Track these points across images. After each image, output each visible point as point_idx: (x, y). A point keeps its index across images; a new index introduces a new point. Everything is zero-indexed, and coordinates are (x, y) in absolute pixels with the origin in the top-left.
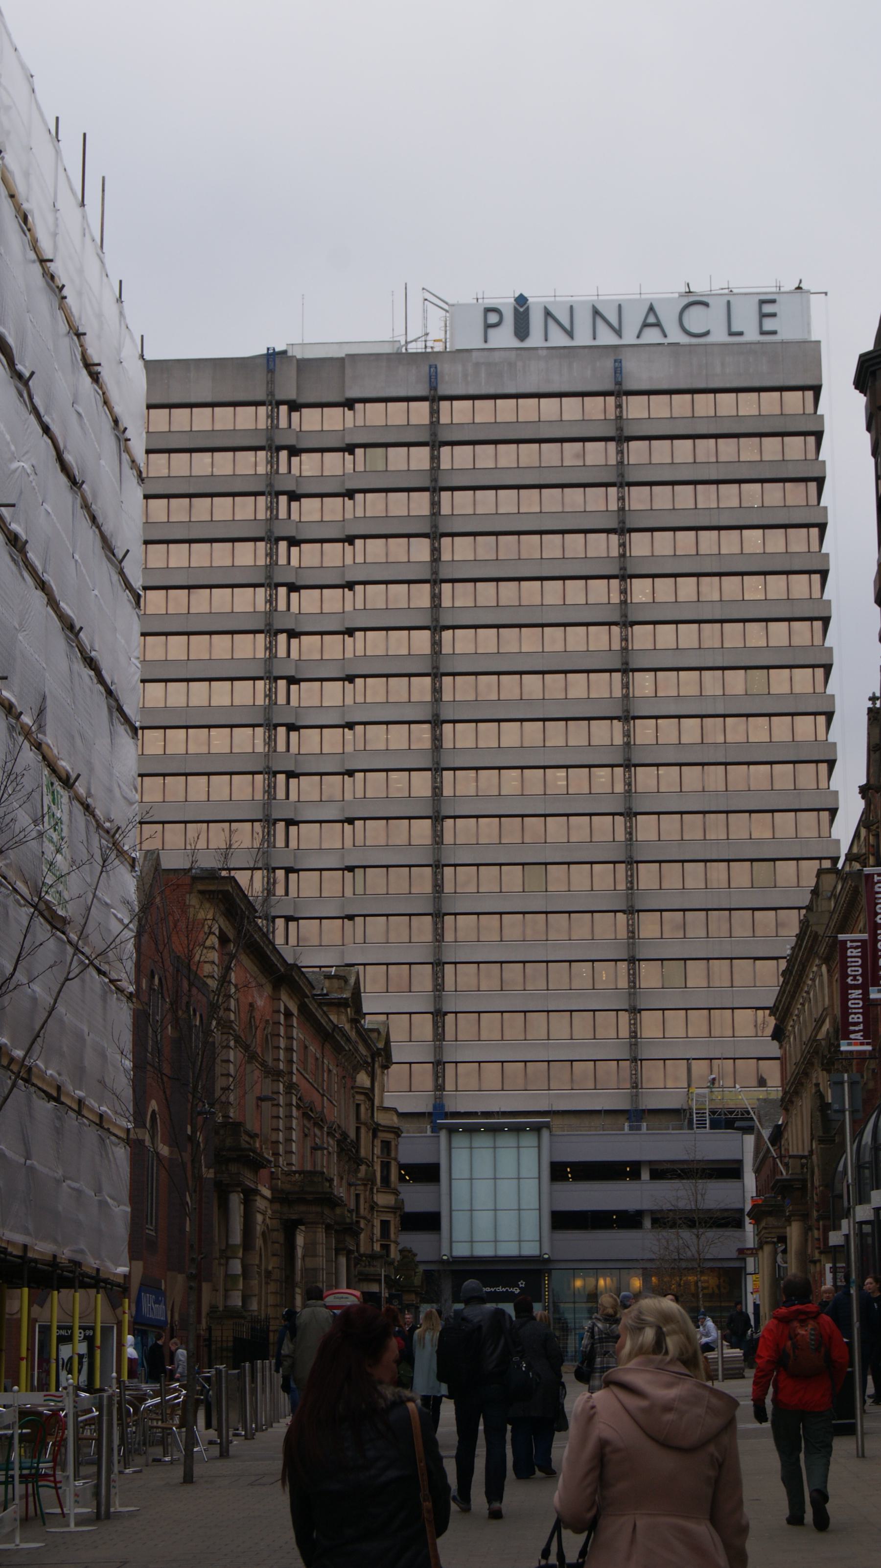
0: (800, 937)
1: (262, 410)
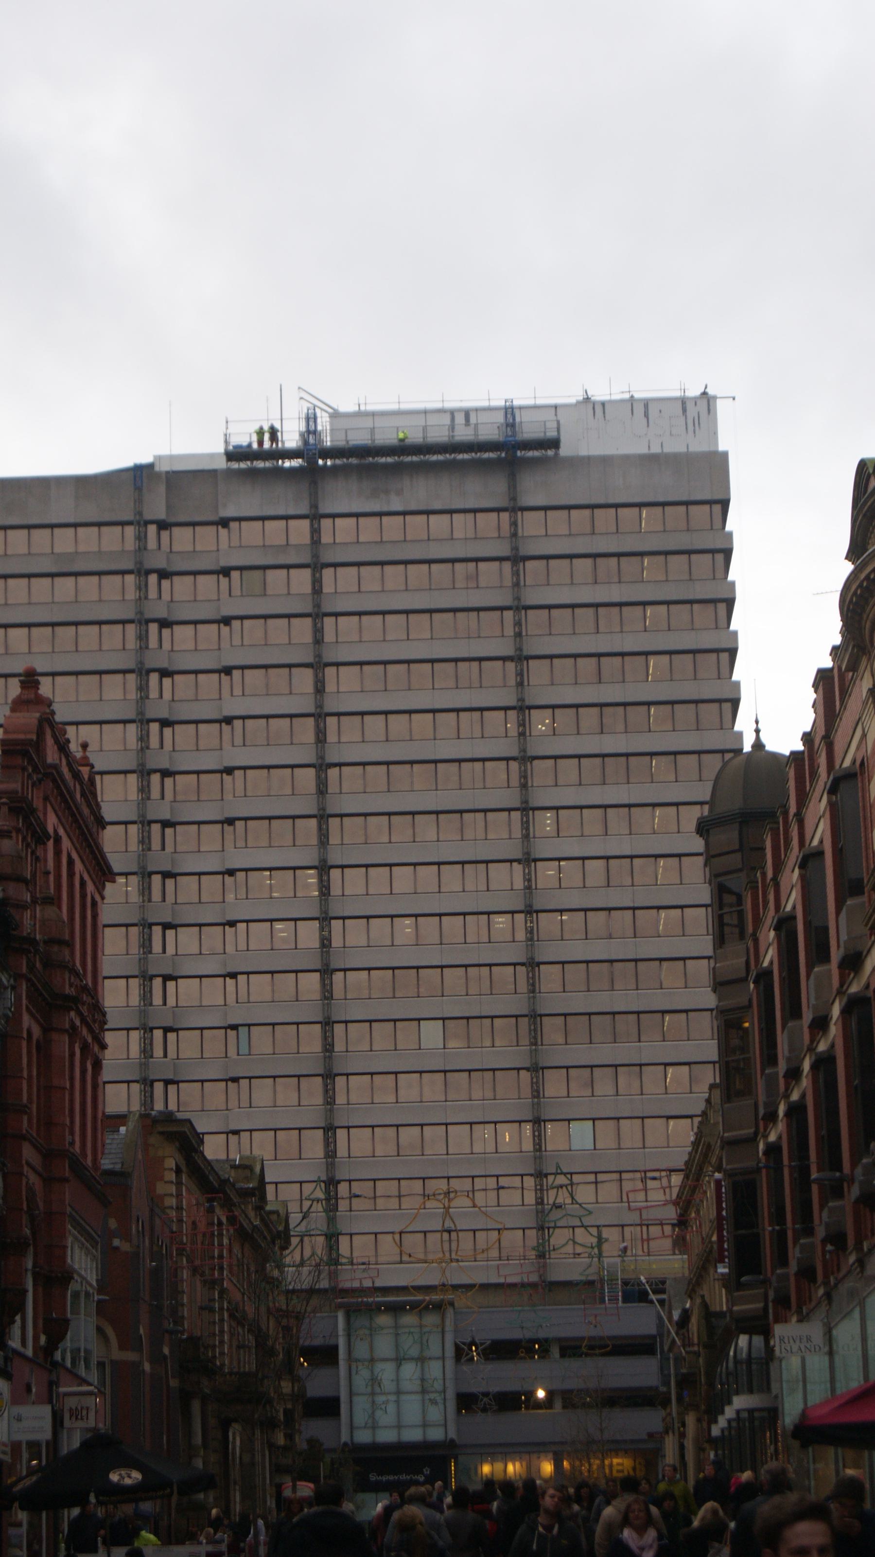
0: (696, 1144)
1: (130, 531)
